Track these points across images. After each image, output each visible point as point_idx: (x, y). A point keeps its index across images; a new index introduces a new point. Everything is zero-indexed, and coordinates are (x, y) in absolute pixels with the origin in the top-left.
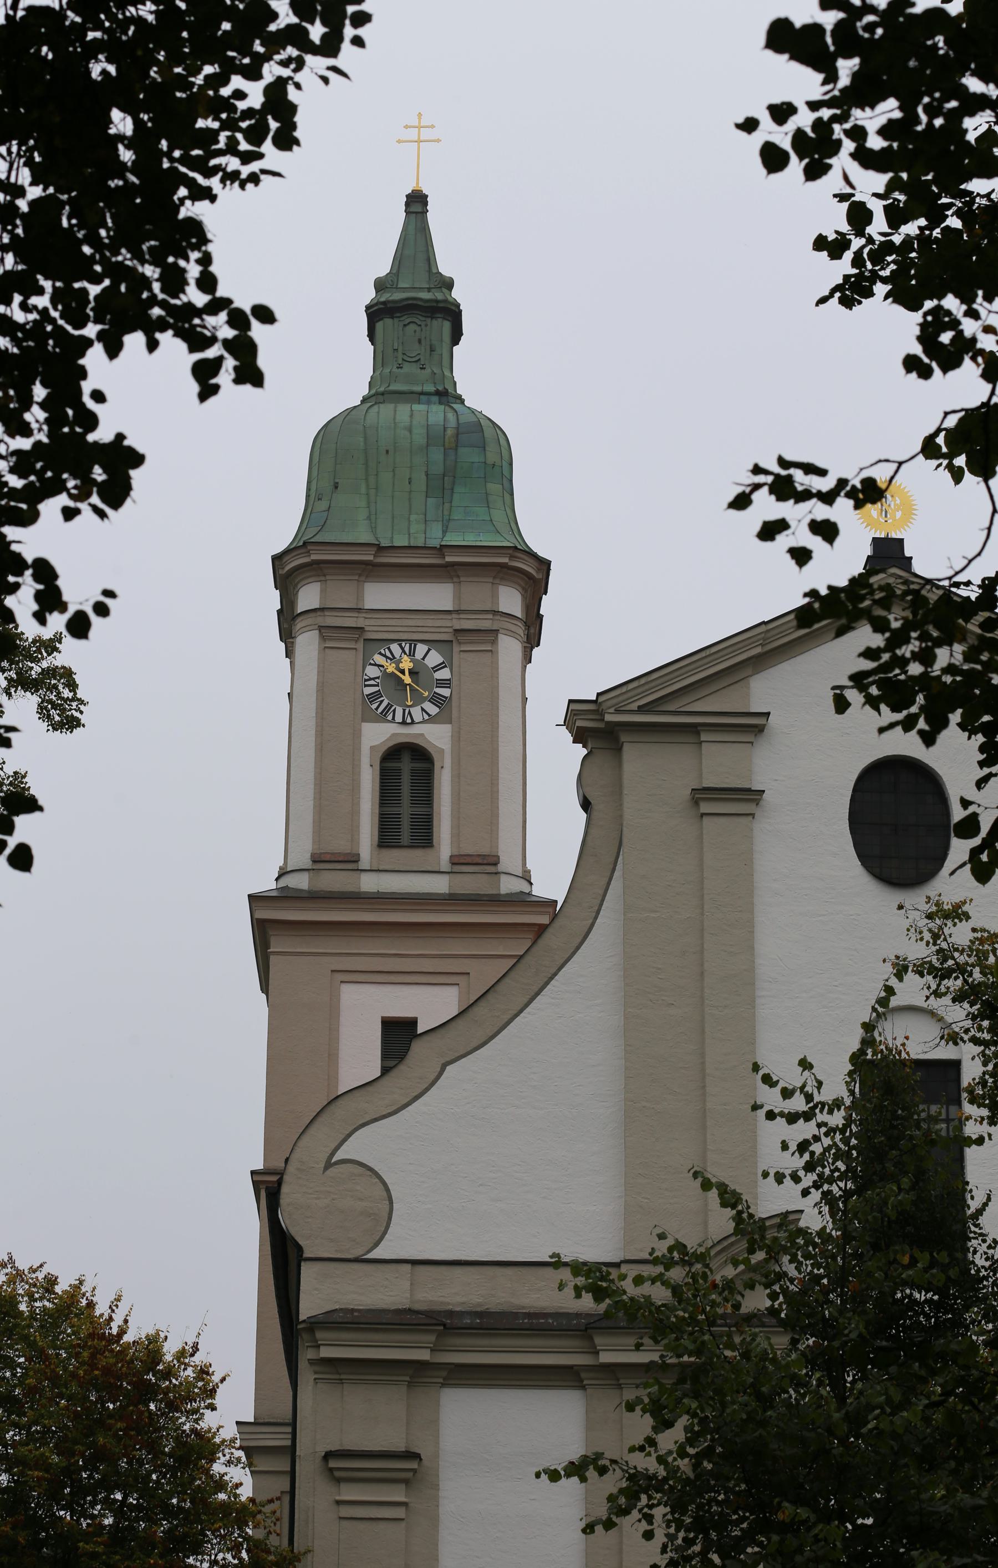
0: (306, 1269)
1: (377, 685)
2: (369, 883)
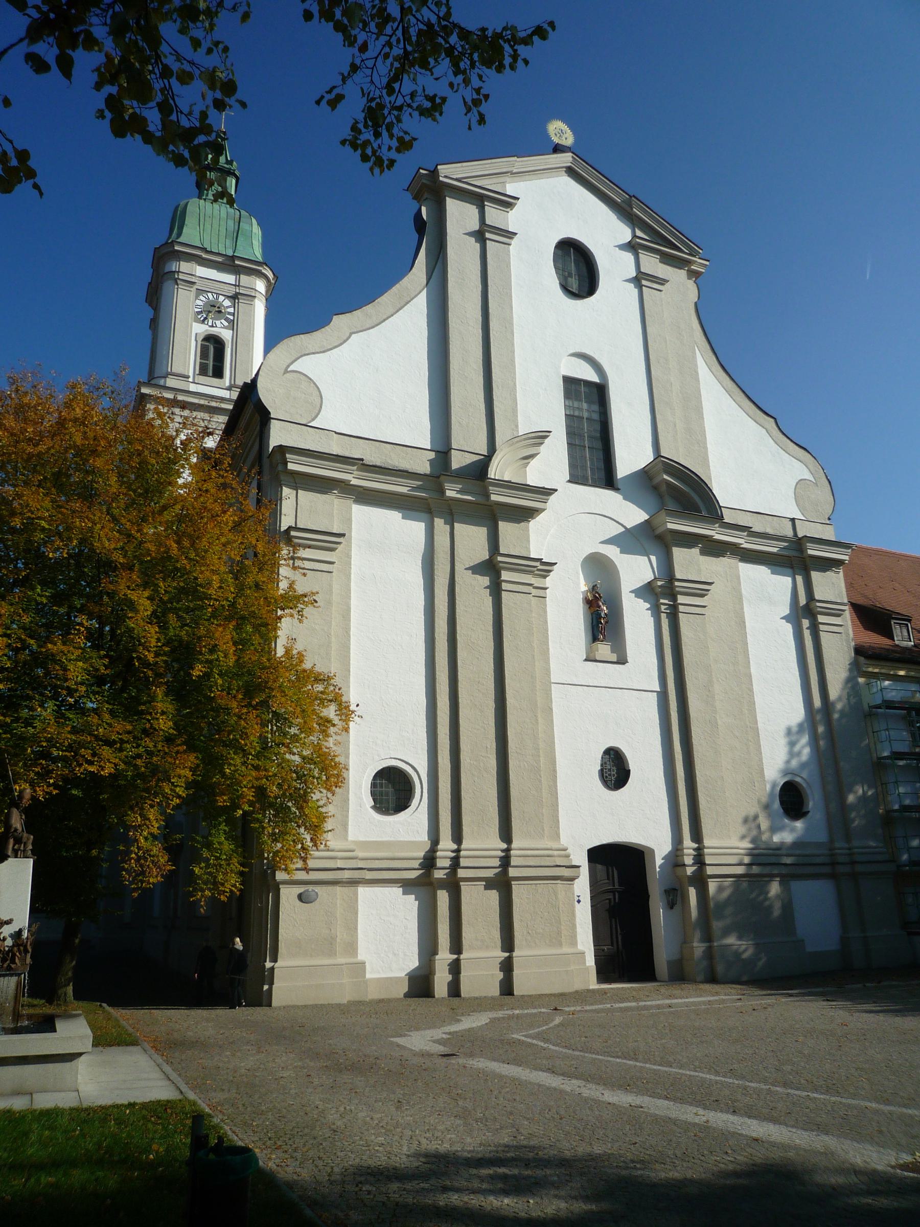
0: (273, 423)
2: (193, 388)
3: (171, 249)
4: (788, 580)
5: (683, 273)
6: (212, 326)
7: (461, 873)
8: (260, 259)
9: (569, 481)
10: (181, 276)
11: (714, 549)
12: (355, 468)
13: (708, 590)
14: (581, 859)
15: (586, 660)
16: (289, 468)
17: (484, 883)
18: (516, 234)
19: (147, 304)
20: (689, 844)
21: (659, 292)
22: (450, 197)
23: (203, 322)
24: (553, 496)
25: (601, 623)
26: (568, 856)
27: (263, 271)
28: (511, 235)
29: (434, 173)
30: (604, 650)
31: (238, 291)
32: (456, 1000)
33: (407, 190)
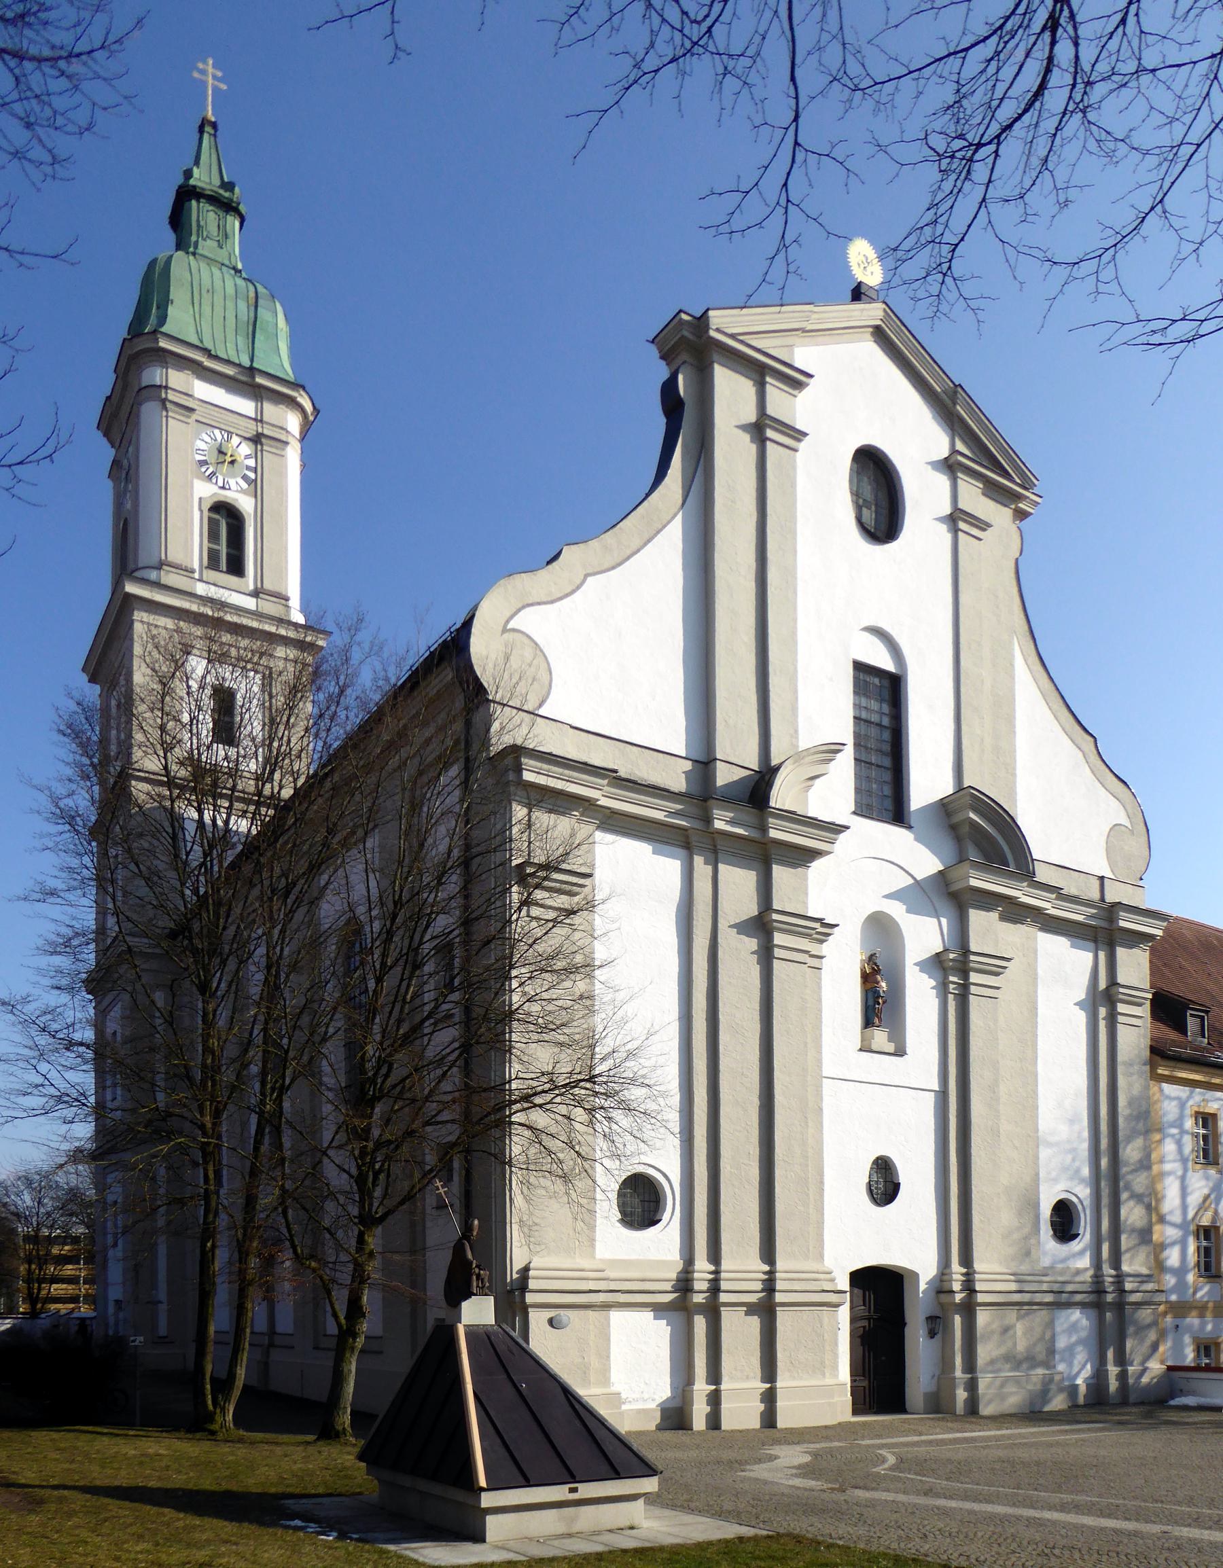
2: (201, 589)
3: (153, 345)
4: (1088, 957)
5: (1007, 513)
6: (223, 488)
7: (723, 1298)
8: (291, 376)
9: (854, 813)
10: (171, 396)
11: (1015, 912)
12: (606, 782)
13: (1005, 968)
14: (844, 1284)
15: (861, 1050)
16: (524, 778)
17: (745, 1309)
18: (805, 434)
19: (100, 434)
20: (957, 1269)
21: (977, 542)
22: (720, 364)
23: (210, 478)
24: (842, 835)
25: (879, 1004)
26: (833, 1280)
27: (299, 399)
28: (799, 435)
29: (702, 321)
30: (880, 1037)
31: (260, 430)
32: (717, 1432)
33: (653, 342)
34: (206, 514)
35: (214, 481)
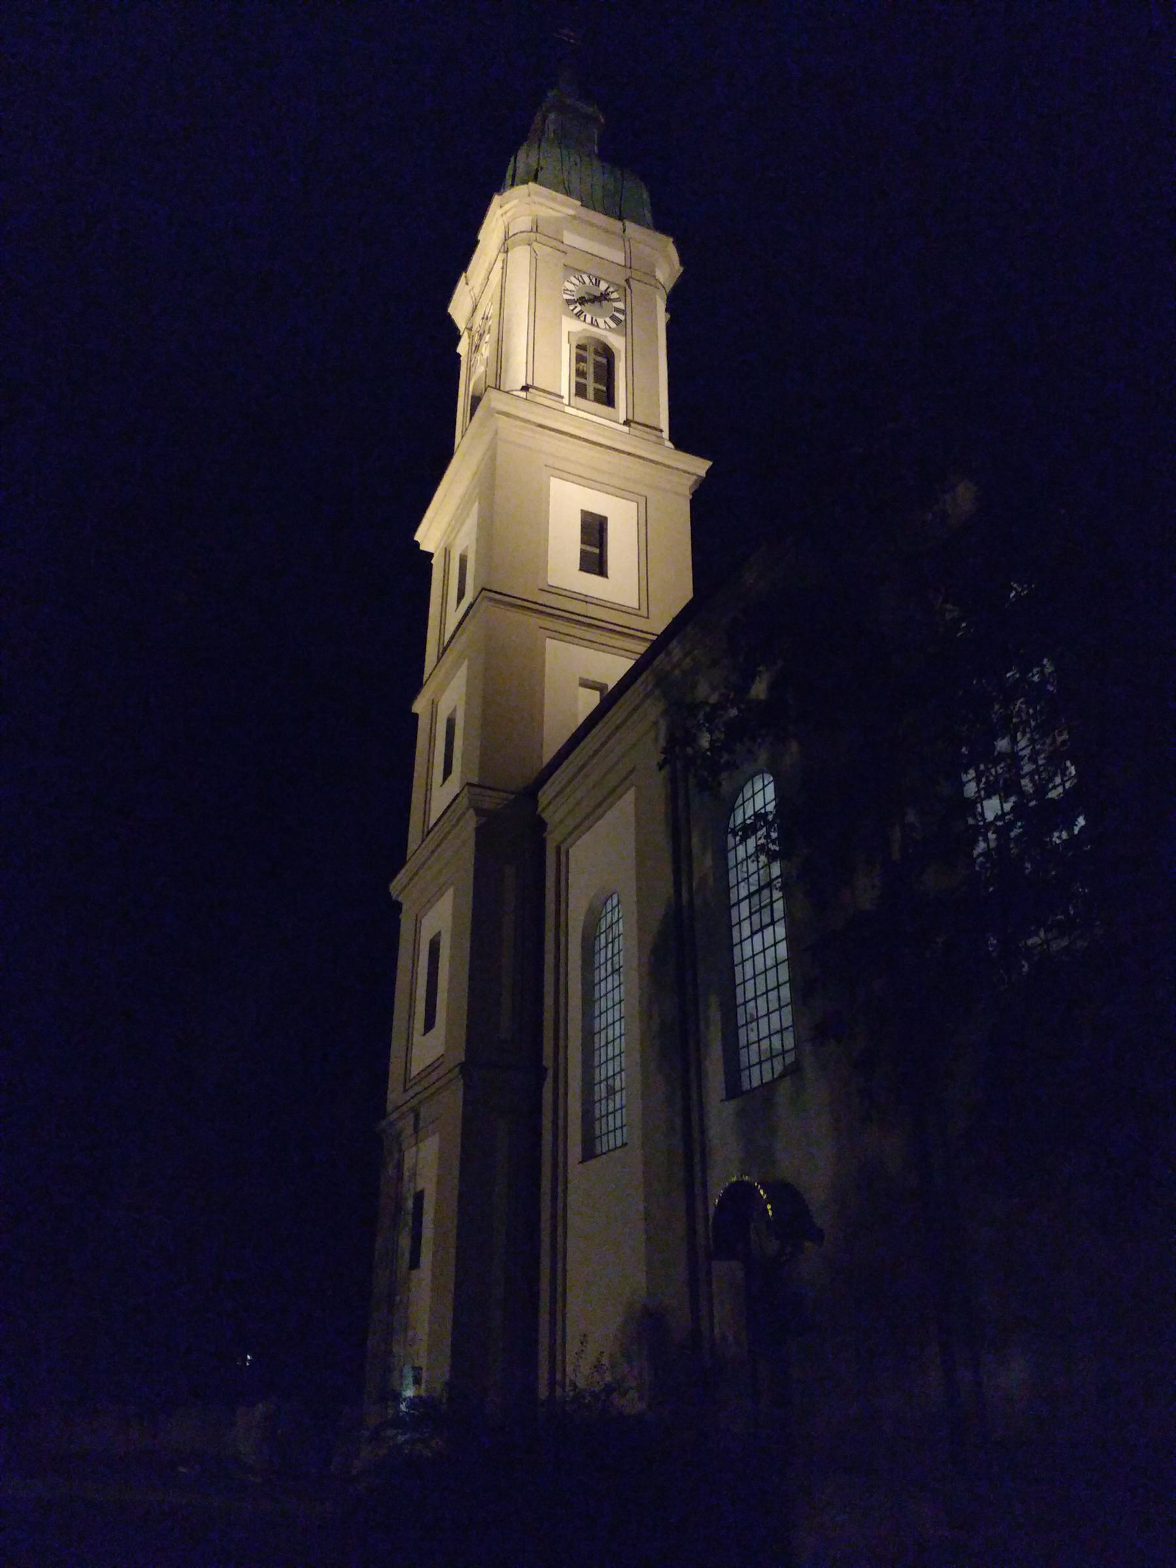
1: (573, 296)
34: (574, 350)
35: (582, 319)
